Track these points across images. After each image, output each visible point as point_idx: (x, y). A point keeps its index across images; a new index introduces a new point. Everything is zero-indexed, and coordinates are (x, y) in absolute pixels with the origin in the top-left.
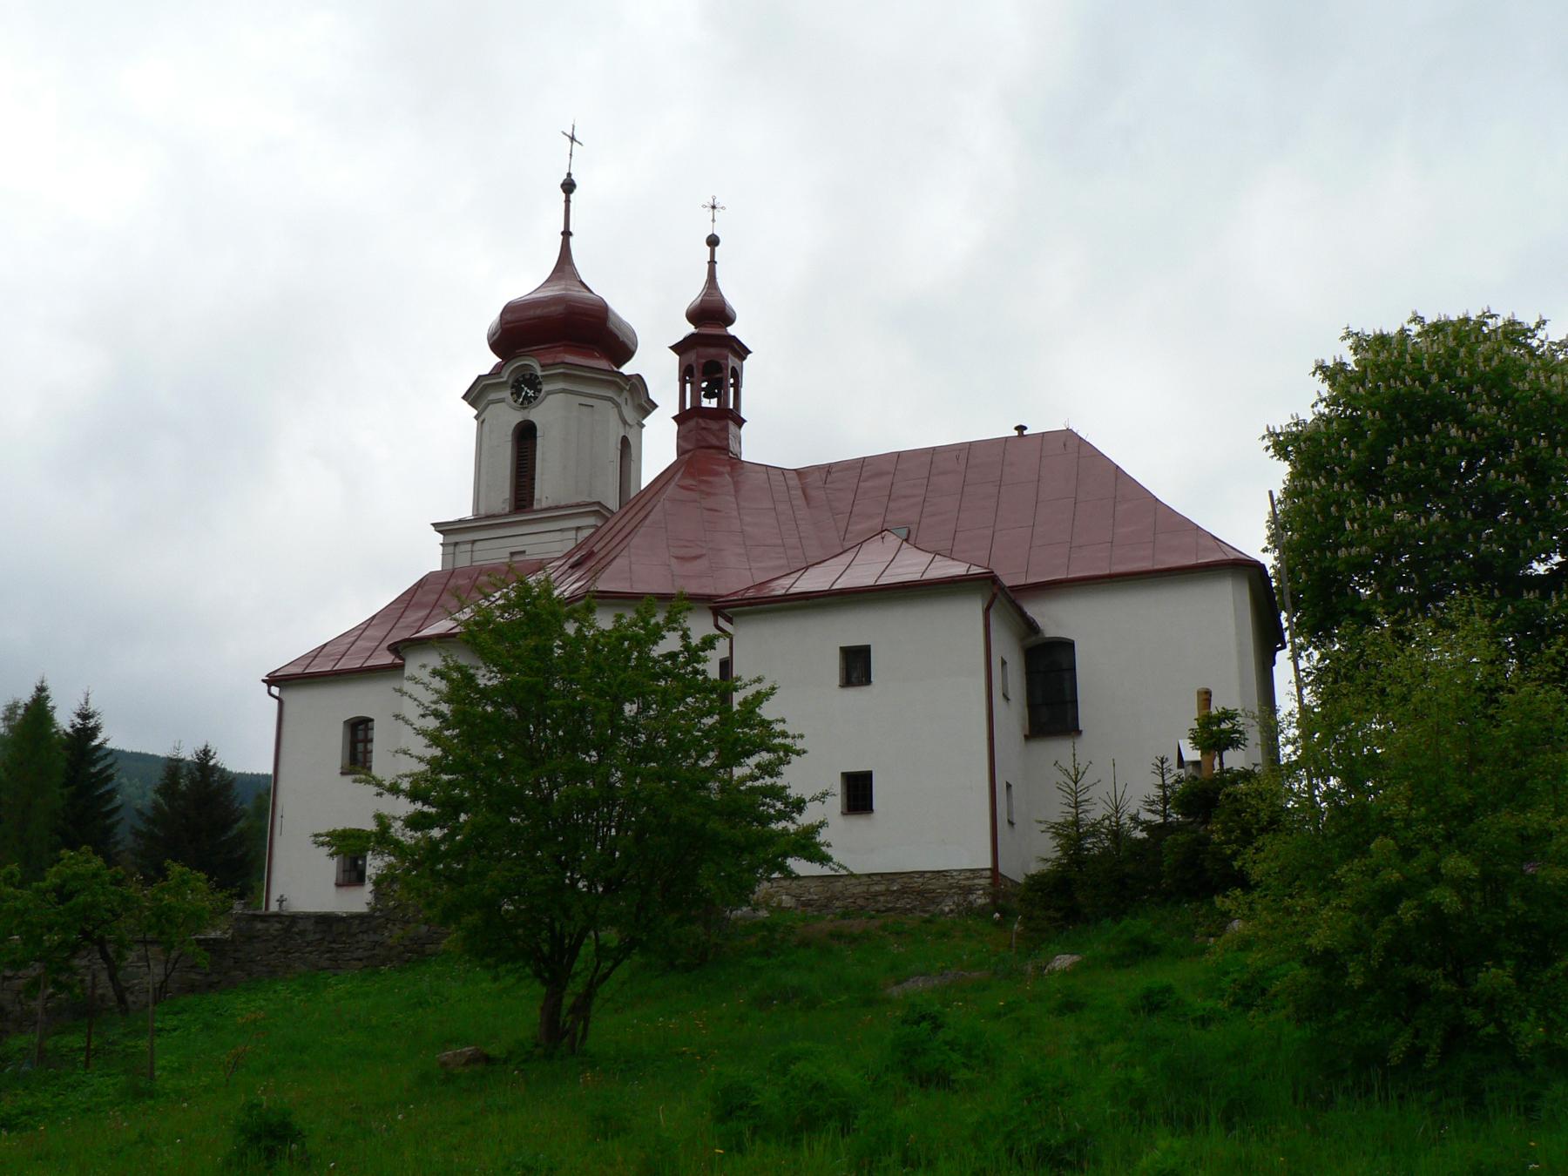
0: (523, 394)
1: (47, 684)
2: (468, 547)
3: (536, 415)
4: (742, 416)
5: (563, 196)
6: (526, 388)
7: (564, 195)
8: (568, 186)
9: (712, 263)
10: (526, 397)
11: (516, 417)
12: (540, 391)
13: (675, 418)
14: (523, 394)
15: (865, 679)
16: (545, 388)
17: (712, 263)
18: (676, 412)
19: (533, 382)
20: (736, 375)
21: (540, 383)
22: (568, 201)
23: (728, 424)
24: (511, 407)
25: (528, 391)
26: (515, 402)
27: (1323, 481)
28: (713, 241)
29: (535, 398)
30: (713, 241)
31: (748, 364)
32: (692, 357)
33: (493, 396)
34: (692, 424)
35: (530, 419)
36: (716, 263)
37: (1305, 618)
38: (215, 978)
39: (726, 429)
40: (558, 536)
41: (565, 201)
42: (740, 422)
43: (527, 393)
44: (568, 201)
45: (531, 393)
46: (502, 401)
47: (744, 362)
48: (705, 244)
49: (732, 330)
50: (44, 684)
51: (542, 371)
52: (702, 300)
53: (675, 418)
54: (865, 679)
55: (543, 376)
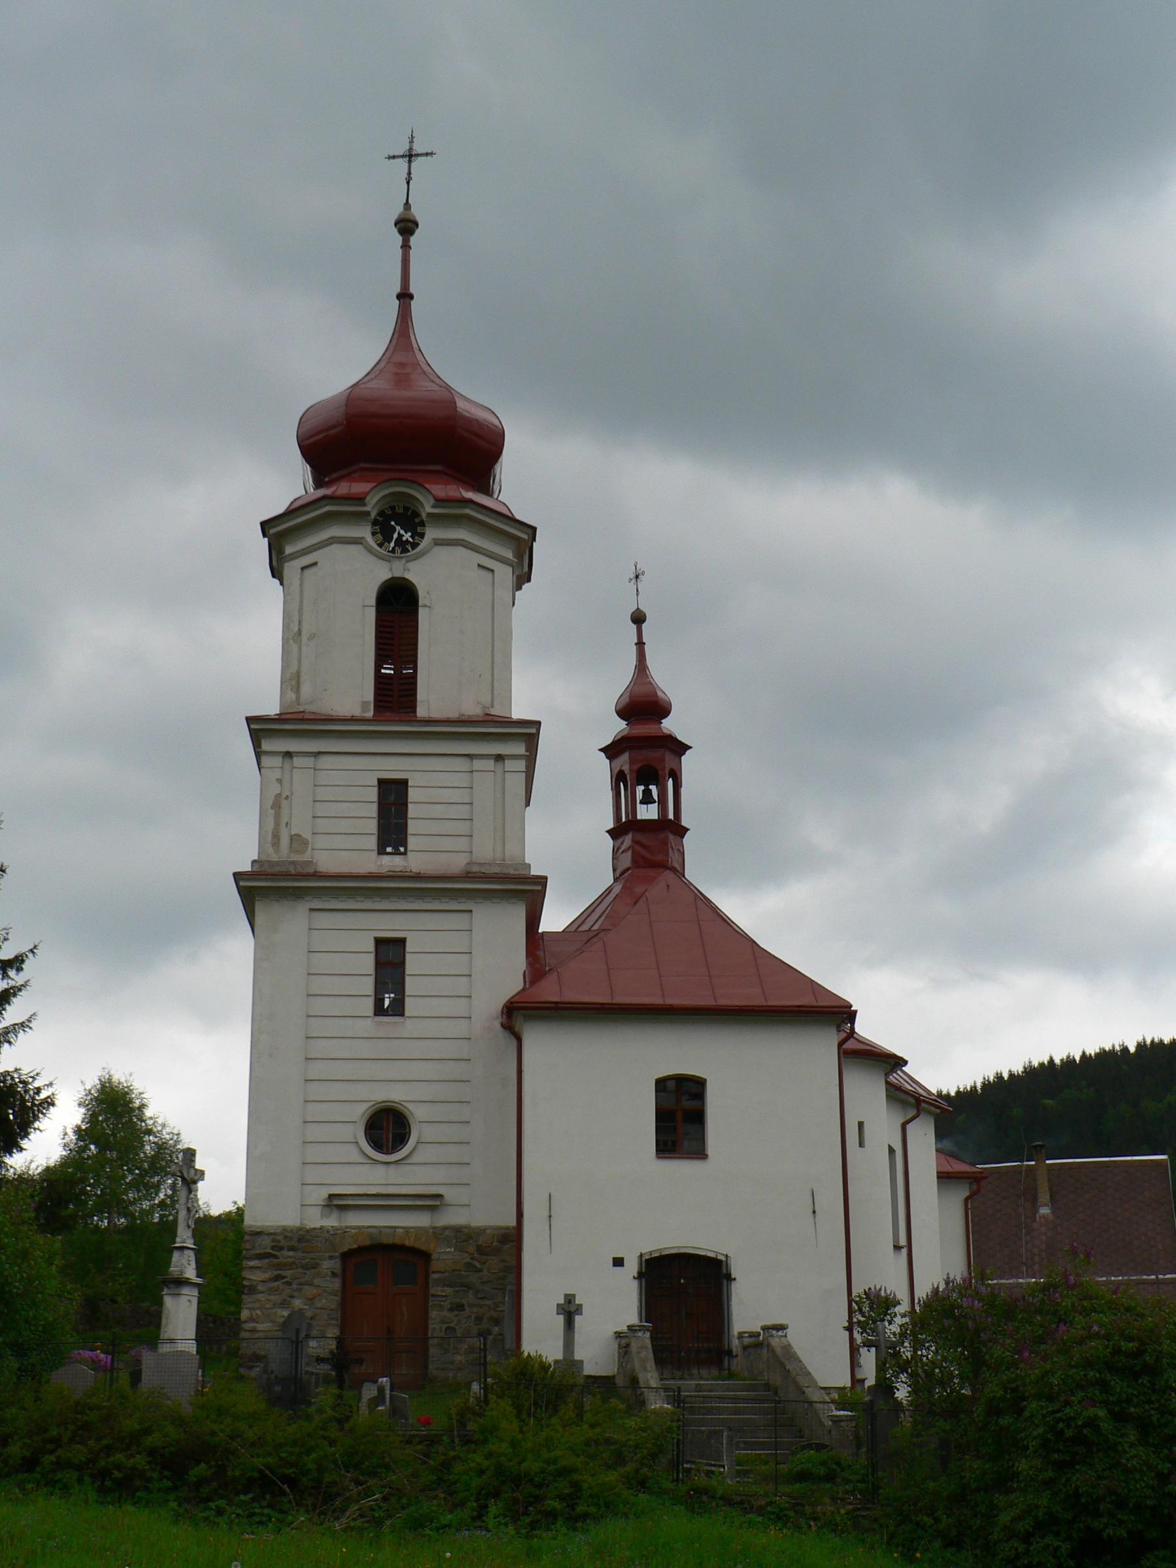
0: (395, 536)
1: (1053, 1055)
2: (309, 761)
3: (420, 573)
4: (683, 824)
5: (399, 239)
6: (398, 528)
7: (400, 238)
8: (406, 226)
9: (640, 644)
10: (400, 542)
11: (382, 572)
12: (422, 535)
13: (609, 832)
14: (395, 536)
16: (431, 533)
17: (640, 644)
19: (413, 521)
21: (422, 524)
22: (406, 246)
23: (667, 838)
24: (370, 550)
25: (402, 532)
26: (380, 545)
27: (127, 1116)
28: (638, 619)
29: (415, 545)
30: (638, 619)
32: (624, 761)
34: (628, 840)
35: (408, 576)
36: (644, 644)
39: (665, 843)
40: (462, 764)
42: (682, 831)
43: (400, 536)
44: (406, 246)
45: (407, 536)
48: (631, 623)
49: (669, 725)
51: (433, 507)
52: (630, 696)
53: (609, 832)
55: (429, 515)
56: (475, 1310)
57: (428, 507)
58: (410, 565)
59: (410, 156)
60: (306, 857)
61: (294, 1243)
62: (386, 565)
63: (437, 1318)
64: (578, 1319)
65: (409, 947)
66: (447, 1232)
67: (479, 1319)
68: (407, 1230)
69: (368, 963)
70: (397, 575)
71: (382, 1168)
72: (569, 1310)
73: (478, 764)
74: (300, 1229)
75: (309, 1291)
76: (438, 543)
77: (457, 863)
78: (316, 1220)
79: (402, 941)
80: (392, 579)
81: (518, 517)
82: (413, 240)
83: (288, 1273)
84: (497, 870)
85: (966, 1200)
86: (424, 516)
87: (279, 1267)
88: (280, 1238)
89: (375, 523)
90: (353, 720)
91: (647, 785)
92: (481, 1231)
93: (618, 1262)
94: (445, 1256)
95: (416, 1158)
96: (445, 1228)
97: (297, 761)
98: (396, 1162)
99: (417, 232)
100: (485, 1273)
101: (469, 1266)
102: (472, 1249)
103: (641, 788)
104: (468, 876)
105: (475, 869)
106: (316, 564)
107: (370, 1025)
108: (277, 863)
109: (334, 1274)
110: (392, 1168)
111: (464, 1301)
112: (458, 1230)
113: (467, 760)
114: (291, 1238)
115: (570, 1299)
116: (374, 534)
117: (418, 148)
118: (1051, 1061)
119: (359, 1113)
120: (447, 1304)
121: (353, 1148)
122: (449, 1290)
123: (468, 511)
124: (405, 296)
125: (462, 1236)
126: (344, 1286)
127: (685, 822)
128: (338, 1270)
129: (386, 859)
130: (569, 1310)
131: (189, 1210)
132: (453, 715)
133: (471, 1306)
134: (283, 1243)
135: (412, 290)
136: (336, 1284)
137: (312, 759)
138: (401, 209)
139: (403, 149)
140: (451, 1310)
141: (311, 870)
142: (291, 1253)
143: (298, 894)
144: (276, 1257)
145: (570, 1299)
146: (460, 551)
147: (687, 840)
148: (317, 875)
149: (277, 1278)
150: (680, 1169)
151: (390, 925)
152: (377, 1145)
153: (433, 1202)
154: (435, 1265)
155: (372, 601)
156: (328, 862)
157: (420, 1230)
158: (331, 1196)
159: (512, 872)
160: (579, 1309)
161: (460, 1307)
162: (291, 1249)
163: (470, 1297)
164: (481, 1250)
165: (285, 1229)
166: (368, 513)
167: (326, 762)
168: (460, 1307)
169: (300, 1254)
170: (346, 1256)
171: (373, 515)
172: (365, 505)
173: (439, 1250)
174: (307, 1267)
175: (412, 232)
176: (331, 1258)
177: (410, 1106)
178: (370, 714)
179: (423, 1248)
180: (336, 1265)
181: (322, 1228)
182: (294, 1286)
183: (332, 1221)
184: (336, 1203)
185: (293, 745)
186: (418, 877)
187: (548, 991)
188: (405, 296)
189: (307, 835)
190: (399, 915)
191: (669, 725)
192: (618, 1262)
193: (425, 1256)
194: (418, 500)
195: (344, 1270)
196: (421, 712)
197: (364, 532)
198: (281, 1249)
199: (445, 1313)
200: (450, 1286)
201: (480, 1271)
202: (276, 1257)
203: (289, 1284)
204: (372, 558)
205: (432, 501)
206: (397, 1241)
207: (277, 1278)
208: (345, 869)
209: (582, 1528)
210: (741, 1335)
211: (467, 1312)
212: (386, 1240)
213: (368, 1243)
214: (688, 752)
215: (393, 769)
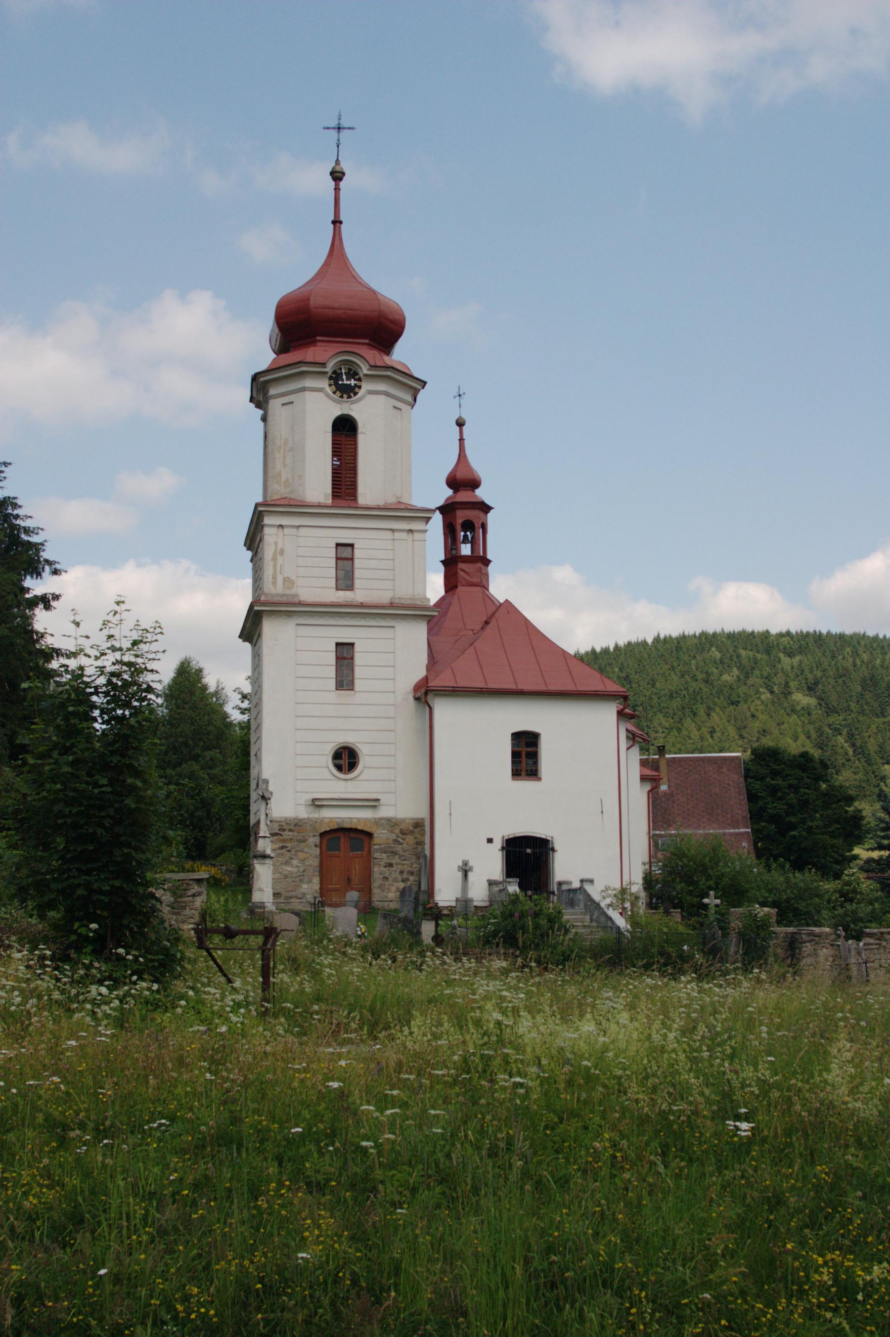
2: (293, 531)
3: (357, 410)
9: (461, 440)
11: (336, 410)
13: (442, 562)
15: (517, 737)
17: (461, 440)
18: (443, 558)
20: (484, 527)
22: (337, 189)
24: (328, 396)
26: (334, 393)
28: (460, 424)
30: (460, 424)
31: (491, 517)
33: (308, 383)
37: (878, 662)
38: (420, 909)
40: (389, 535)
41: (335, 189)
42: (487, 562)
44: (337, 189)
46: (320, 390)
47: (489, 515)
49: (481, 493)
50: (63, 573)
51: (368, 370)
54: (517, 737)
55: (366, 375)
56: (399, 867)
57: (365, 370)
58: (353, 406)
59: (339, 128)
60: (293, 592)
61: (292, 827)
62: (339, 406)
63: (378, 871)
64: (470, 874)
65: (357, 648)
66: (382, 821)
67: (402, 872)
68: (359, 819)
69: (331, 658)
70: (346, 412)
71: (343, 783)
72: (465, 870)
73: (397, 535)
74: (296, 819)
75: (302, 855)
76: (370, 392)
77: (384, 597)
78: (303, 813)
79: (352, 645)
80: (342, 415)
81: (416, 375)
82: (342, 184)
83: (289, 845)
84: (410, 602)
85: (649, 792)
86: (361, 375)
87: (283, 841)
88: (283, 824)
89: (331, 378)
90: (319, 506)
91: (465, 532)
92: (403, 820)
93: (490, 841)
94: (381, 836)
95: (362, 777)
96: (381, 819)
97: (286, 531)
98: (351, 779)
99: (345, 178)
100: (405, 845)
101: (395, 841)
102: (397, 831)
103: (462, 534)
104: (392, 605)
105: (397, 601)
106: (292, 403)
107: (334, 696)
108: (277, 595)
109: (316, 846)
110: (349, 783)
111: (393, 862)
112: (389, 820)
113: (390, 533)
114: (290, 824)
115: (465, 863)
116: (330, 385)
117: (344, 124)
118: (593, 650)
119: (329, 750)
120: (383, 864)
121: (326, 770)
122: (384, 855)
123: (389, 373)
124: (337, 222)
125: (391, 823)
126: (321, 853)
127: (489, 557)
128: (318, 844)
129: (341, 594)
130: (465, 870)
131: (267, 815)
132: (381, 503)
133: (397, 864)
134: (285, 827)
135: (342, 218)
136: (318, 851)
137: (295, 530)
138: (333, 164)
139: (334, 124)
140: (386, 867)
141: (297, 600)
142: (291, 833)
143: (289, 614)
144: (281, 835)
145: (465, 863)
146: (382, 398)
147: (491, 568)
148: (300, 604)
149: (283, 847)
150: (526, 786)
151: (345, 635)
152: (339, 768)
153: (373, 803)
154: (376, 840)
155: (330, 429)
156: (306, 595)
157: (367, 820)
158: (314, 800)
159: (419, 603)
160: (471, 869)
161: (391, 865)
162: (291, 830)
163: (396, 860)
164: (403, 832)
165: (286, 819)
166: (326, 373)
167: (303, 531)
168: (391, 865)
169: (295, 834)
170: (322, 835)
171: (330, 374)
172: (325, 367)
173: (378, 831)
174: (300, 841)
175: (341, 179)
176: (314, 836)
177: (359, 745)
178: (329, 501)
179: (369, 830)
180: (317, 840)
181: (308, 818)
182: (293, 853)
183: (316, 815)
184: (316, 804)
185: (284, 521)
186: (362, 605)
187: (443, 680)
188: (337, 222)
189: (293, 578)
190: (344, 628)
191: (481, 493)
192: (490, 841)
193: (370, 835)
194: (358, 365)
195: (321, 843)
196: (361, 501)
197: (324, 383)
198: (284, 830)
199: (382, 869)
200: (385, 852)
201: (402, 844)
202: (281, 835)
203: (289, 851)
204: (330, 401)
205: (368, 367)
206: (353, 826)
207: (283, 847)
208: (317, 599)
209: (43, 958)
210: (560, 884)
211: (395, 868)
212: (347, 826)
213: (336, 827)
214: (492, 511)
215: (345, 537)
